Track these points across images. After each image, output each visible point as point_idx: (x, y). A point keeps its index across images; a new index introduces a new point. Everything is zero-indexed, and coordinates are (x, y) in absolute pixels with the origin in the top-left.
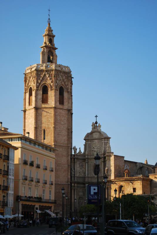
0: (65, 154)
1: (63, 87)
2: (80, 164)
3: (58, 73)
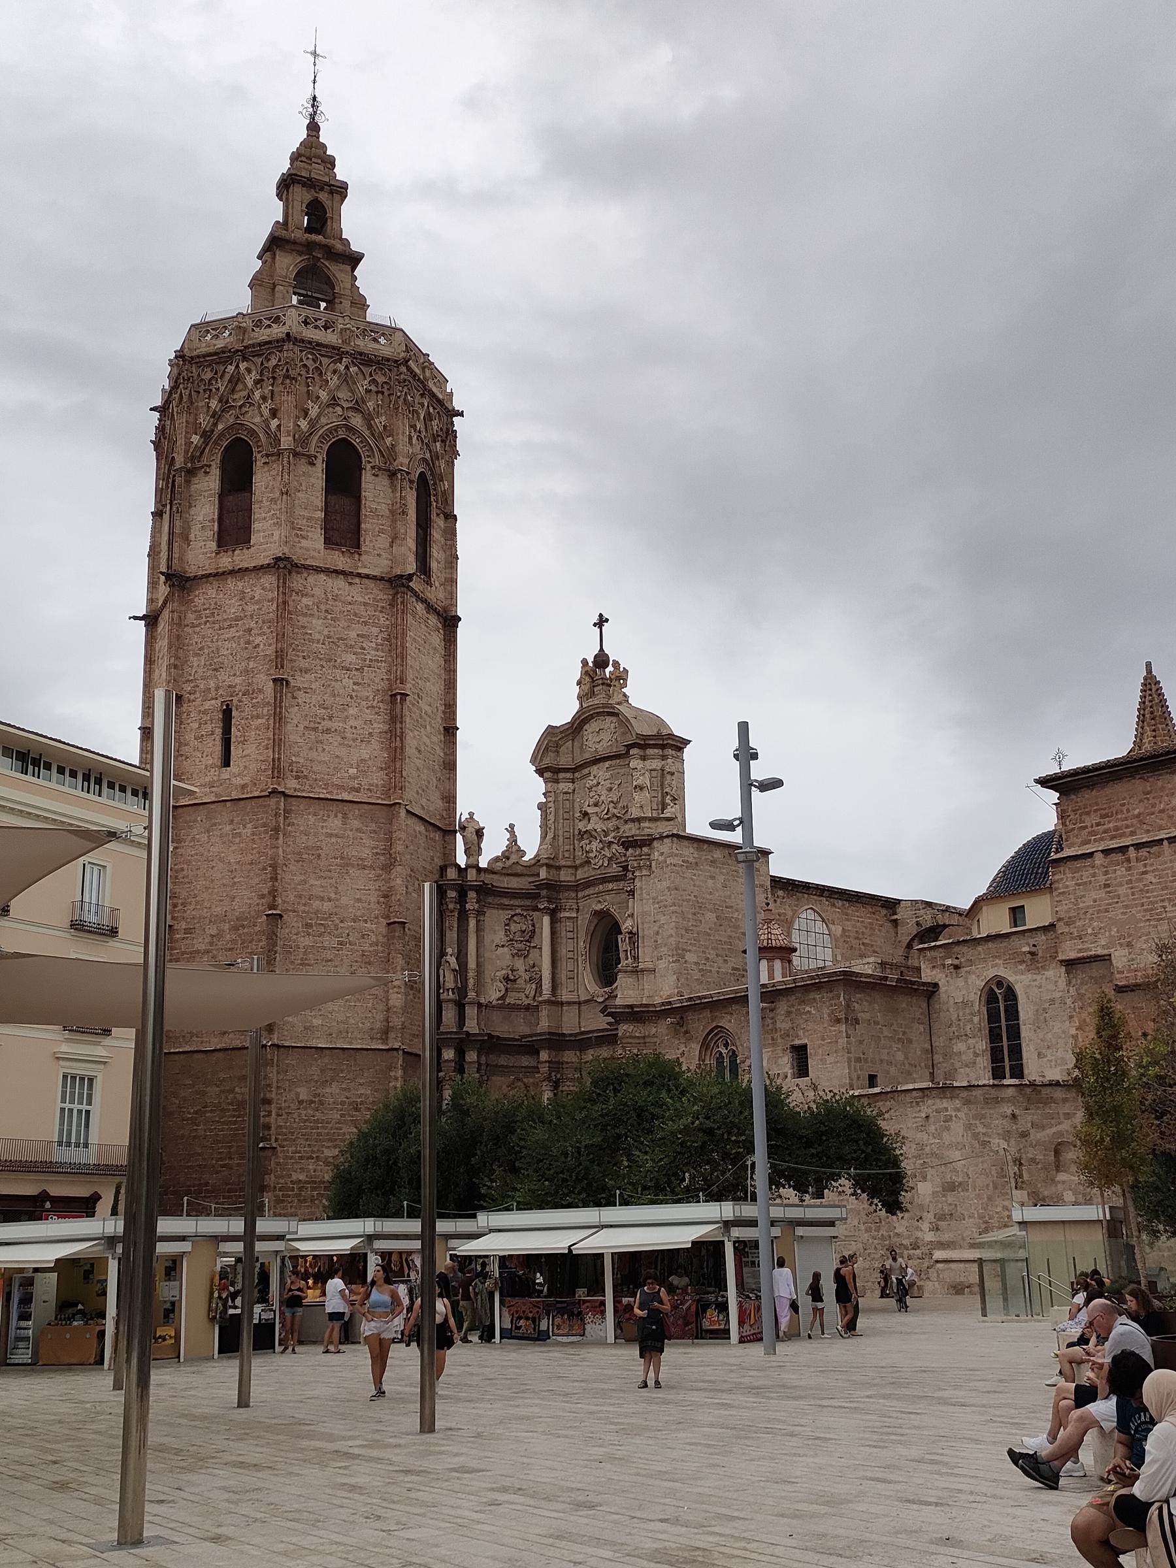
0: (366, 853)
1: (355, 441)
2: (514, 927)
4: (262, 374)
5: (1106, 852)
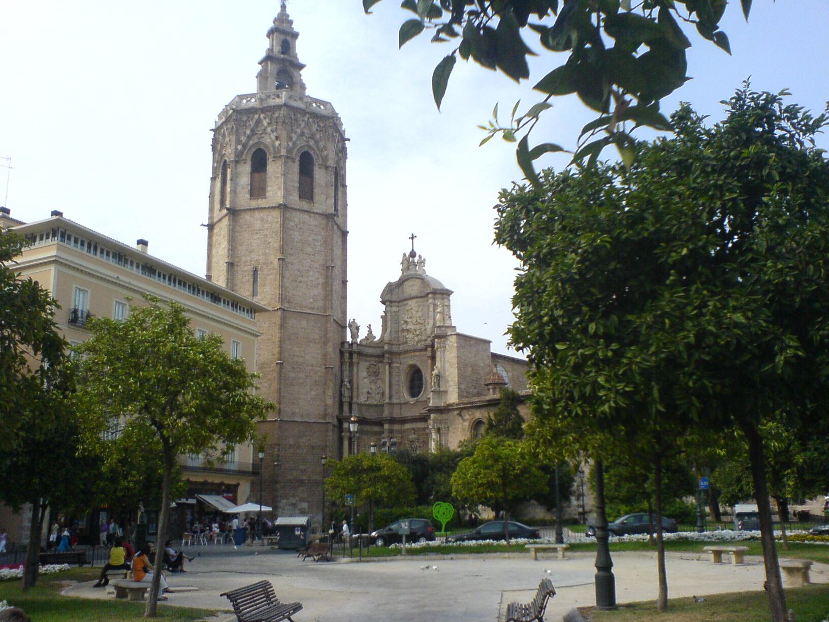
0: (316, 336)
1: (312, 152)
2: (371, 370)
4: (270, 120)
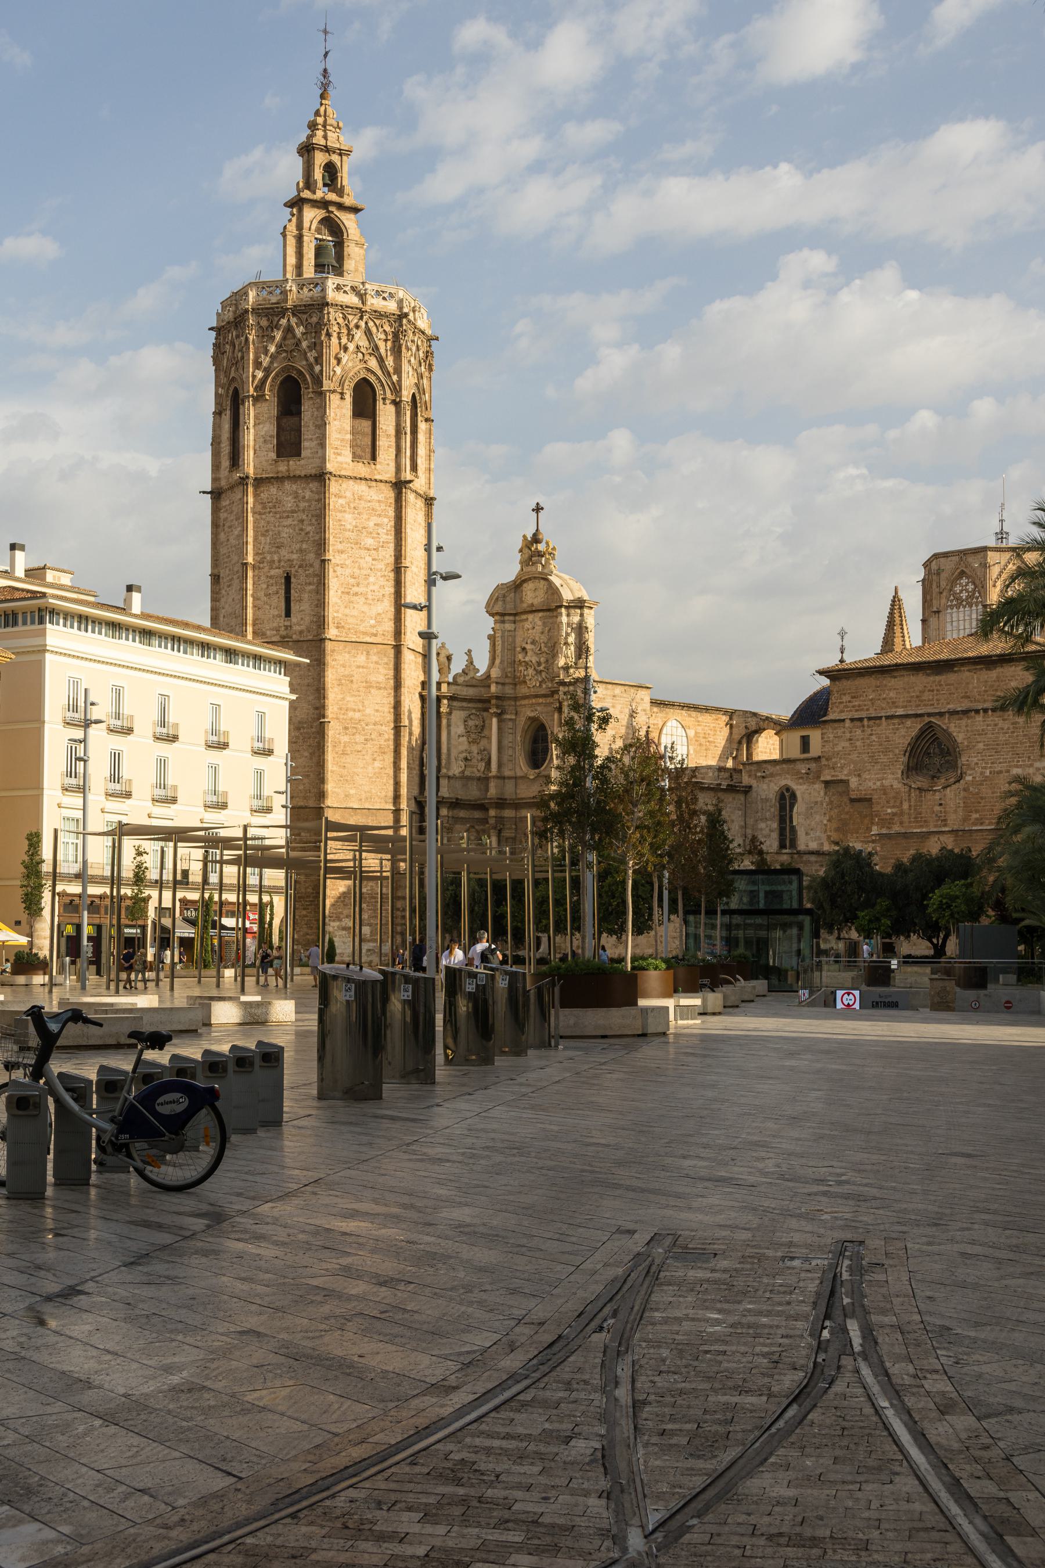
0: (381, 678)
1: (372, 379)
3: (345, 318)
5: (852, 720)
